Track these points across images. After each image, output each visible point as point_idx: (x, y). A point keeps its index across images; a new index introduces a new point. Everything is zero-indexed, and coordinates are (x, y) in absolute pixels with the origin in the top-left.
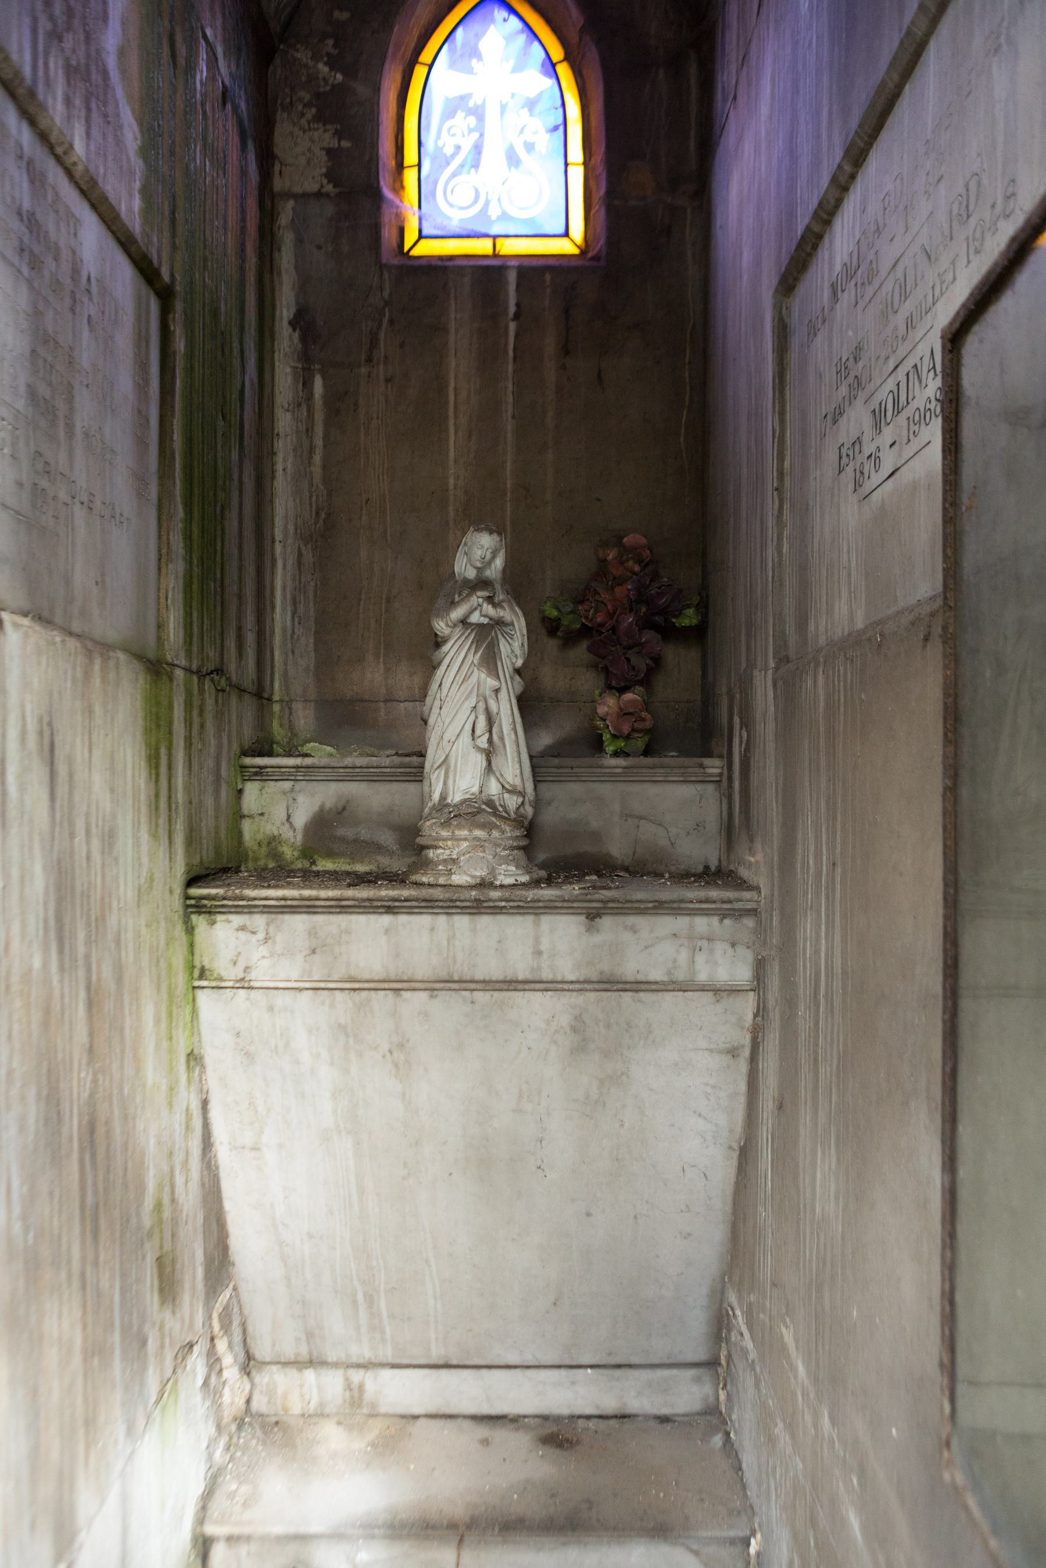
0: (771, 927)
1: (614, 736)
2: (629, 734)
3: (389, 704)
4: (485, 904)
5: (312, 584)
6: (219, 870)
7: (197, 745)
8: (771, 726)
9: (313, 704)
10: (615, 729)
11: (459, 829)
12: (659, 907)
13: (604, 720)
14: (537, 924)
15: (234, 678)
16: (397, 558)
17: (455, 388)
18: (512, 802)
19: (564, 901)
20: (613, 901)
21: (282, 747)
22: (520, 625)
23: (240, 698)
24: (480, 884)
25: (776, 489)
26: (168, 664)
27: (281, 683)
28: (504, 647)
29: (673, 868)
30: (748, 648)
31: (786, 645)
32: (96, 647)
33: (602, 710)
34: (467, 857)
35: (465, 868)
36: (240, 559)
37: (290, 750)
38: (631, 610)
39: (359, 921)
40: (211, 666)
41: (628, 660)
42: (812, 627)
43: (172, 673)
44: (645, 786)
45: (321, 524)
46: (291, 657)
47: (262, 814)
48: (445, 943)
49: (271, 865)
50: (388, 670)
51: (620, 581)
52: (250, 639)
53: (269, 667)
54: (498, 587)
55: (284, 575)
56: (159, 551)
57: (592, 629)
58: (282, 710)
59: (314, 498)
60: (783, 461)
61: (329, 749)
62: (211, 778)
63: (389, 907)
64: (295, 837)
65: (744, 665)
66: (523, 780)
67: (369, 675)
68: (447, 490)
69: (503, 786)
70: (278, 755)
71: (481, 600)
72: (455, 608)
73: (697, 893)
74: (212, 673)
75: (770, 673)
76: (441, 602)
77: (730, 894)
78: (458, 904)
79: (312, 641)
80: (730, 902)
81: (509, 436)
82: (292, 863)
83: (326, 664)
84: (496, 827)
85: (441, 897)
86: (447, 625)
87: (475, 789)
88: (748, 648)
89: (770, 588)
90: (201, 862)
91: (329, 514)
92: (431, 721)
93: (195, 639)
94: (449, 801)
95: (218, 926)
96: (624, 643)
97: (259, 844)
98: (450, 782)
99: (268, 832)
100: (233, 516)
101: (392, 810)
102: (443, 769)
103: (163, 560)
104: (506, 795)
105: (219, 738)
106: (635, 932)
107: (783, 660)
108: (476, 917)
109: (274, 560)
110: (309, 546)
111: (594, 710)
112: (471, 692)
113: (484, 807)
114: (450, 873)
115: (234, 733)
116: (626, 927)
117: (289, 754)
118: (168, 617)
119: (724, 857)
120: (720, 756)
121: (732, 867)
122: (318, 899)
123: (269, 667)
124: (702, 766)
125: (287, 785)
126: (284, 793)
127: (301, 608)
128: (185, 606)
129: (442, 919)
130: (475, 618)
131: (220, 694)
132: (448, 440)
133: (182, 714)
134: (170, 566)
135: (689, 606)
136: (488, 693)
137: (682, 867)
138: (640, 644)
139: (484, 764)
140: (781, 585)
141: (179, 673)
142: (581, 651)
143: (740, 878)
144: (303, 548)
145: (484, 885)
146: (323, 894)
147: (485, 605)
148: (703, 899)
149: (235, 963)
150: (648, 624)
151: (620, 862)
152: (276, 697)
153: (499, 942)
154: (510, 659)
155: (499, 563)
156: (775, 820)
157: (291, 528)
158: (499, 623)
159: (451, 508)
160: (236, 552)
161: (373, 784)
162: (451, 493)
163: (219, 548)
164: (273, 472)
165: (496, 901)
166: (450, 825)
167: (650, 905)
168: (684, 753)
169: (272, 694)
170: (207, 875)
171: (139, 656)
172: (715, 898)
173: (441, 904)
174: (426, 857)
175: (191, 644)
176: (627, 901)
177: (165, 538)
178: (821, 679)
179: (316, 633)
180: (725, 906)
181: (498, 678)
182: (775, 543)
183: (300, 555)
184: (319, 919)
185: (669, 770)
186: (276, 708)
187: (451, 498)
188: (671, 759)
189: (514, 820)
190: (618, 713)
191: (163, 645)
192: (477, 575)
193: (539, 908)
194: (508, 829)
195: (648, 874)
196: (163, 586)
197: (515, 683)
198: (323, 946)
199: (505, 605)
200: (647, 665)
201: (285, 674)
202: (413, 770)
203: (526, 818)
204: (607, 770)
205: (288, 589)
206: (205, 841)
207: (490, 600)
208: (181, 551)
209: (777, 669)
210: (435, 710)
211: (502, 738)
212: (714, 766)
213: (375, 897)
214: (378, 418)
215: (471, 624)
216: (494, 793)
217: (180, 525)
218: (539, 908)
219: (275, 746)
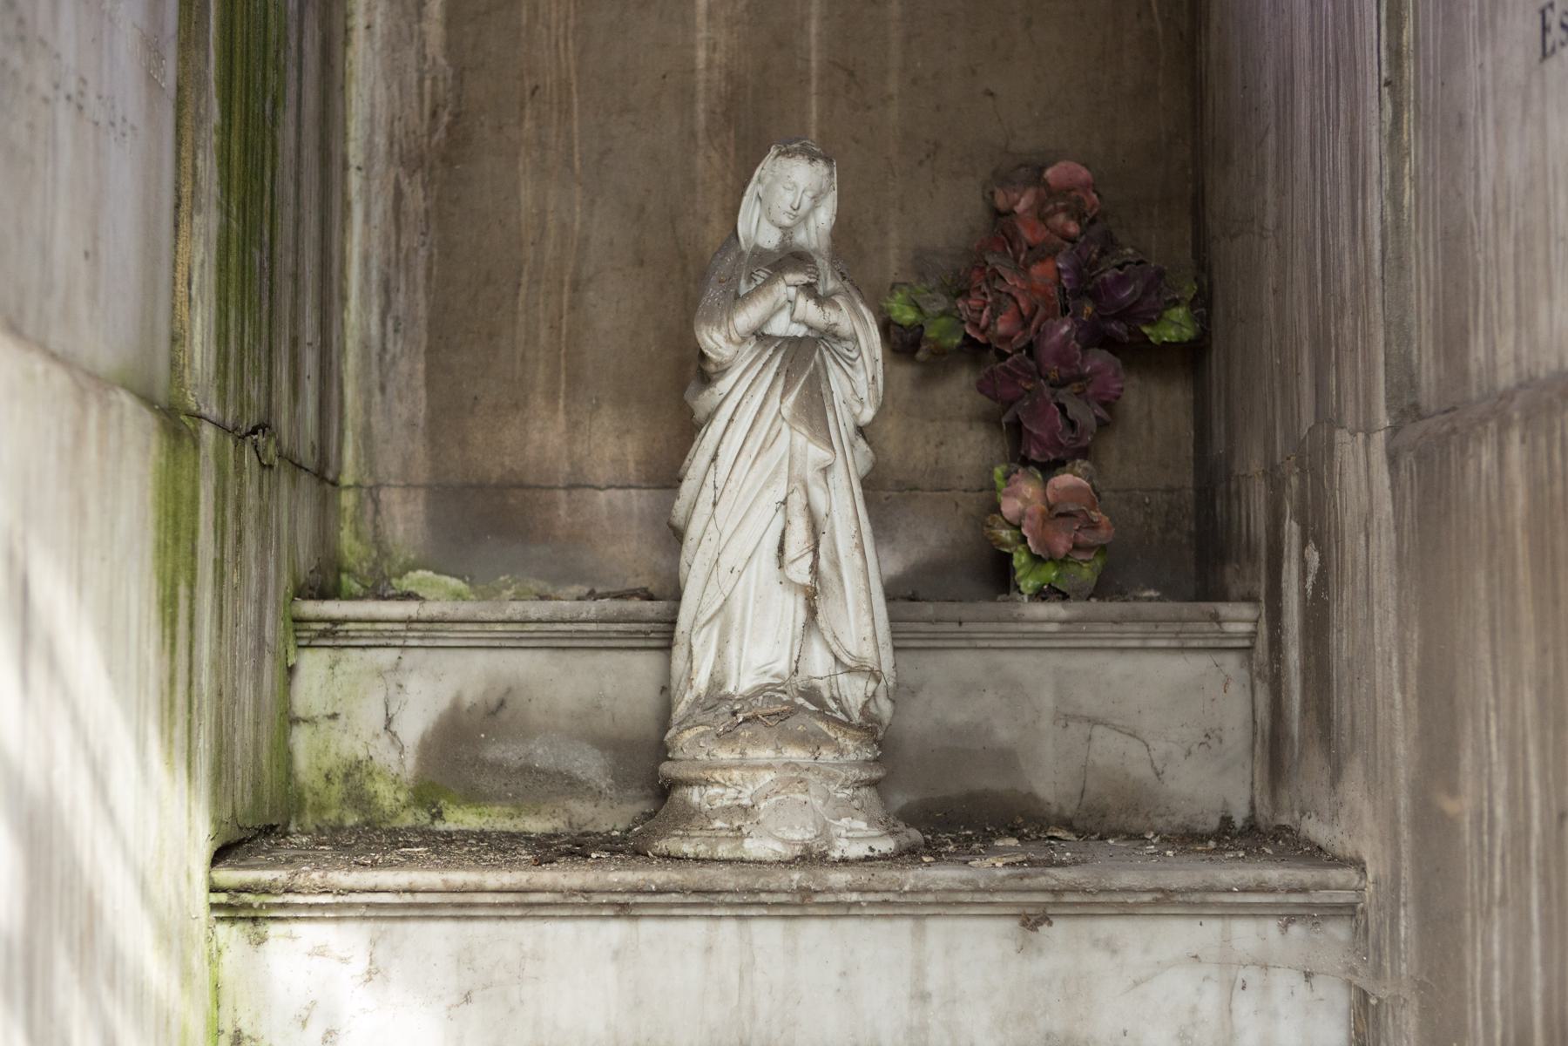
0: (1394, 942)
3: (576, 494)
4: (819, 898)
5: (422, 252)
6: (273, 828)
7: (233, 577)
8: (1384, 544)
9: (422, 493)
10: (1038, 545)
11: (756, 746)
12: (1165, 901)
13: (1019, 528)
14: (919, 937)
15: (285, 443)
16: (593, 202)
18: (855, 691)
19: (977, 890)
20: (1074, 890)
21: (360, 579)
22: (871, 339)
23: (294, 480)
24: (803, 858)
25: (1388, 84)
26: (190, 415)
27: (357, 449)
28: (837, 379)
29: (1160, 823)
30: (1319, 388)
31: (1414, 386)
32: (92, 382)
33: (1010, 507)
34: (775, 803)
35: (771, 826)
36: (298, 204)
37: (375, 587)
39: (561, 935)
40: (252, 419)
42: (1478, 351)
43: (197, 431)
44: (1101, 658)
45: (441, 134)
46: (377, 397)
47: (334, 716)
48: (735, 978)
49: (352, 819)
50: (573, 426)
51: (1040, 253)
52: (310, 360)
53: (335, 419)
54: (823, 264)
55: (367, 236)
56: (177, 190)
57: (988, 346)
58: (360, 504)
59: (428, 83)
60: (1400, 31)
61: (454, 583)
62: (251, 644)
63: (624, 906)
64: (401, 762)
65: (1308, 419)
66: (877, 648)
67: (535, 436)
68: (693, 71)
69: (836, 659)
70: (353, 597)
71: (792, 291)
73: (1239, 873)
74: (254, 431)
75: (1379, 438)
76: (713, 293)
77: (1306, 875)
78: (764, 897)
79: (421, 366)
80: (1303, 890)
82: (395, 815)
83: (447, 416)
84: (829, 741)
85: (731, 885)
86: (729, 339)
87: (783, 666)
88: (1319, 388)
89: (1378, 273)
90: (234, 815)
91: (456, 116)
92: (694, 531)
93: (232, 364)
94: (730, 689)
95: (271, 946)
96: (1053, 375)
97: (328, 778)
98: (732, 650)
99: (346, 751)
100: (288, 117)
101: (599, 707)
102: (717, 623)
103: (185, 207)
104: (843, 679)
105: (263, 564)
106: (1114, 952)
107: (1407, 412)
108: (798, 925)
109: (347, 206)
110: (418, 177)
111: (996, 509)
112: (776, 473)
113: (800, 701)
114: (738, 834)
115: (284, 551)
116: (1095, 943)
117: (377, 593)
118: (191, 320)
119: (1262, 802)
120: (1250, 598)
121: (1284, 820)
122: (480, 890)
123: (335, 419)
124: (1216, 618)
125: (386, 657)
126: (380, 674)
127: (400, 301)
128: (219, 299)
129: (728, 929)
130: (781, 326)
131: (266, 472)
133: (211, 515)
134: (197, 219)
136: (811, 474)
137: (1178, 820)
138: (1081, 377)
139: (802, 615)
140: (1401, 267)
141: (208, 433)
142: (960, 388)
143: (1309, 842)
144: (405, 183)
145: (810, 858)
146: (492, 879)
147: (801, 301)
148: (1253, 884)
149: (304, 1023)
150: (1096, 337)
151: (1054, 810)
152: (347, 478)
153: (844, 974)
154: (850, 409)
155: (825, 216)
156: (1400, 726)
157: (381, 140)
158: (828, 336)
160: (291, 190)
161: (560, 654)
162: (701, 76)
163: (267, 183)
164: (347, 31)
166: (735, 738)
167: (1147, 898)
168: (1170, 592)
169: (339, 473)
170: (240, 843)
171: (146, 399)
172: (1274, 883)
173: (729, 898)
174: (685, 802)
175: (225, 376)
176: (1102, 891)
177: (188, 163)
178: (1516, 452)
179: (429, 351)
180: (1295, 898)
181: (831, 445)
182: (1387, 185)
183: (399, 195)
184: (479, 931)
186: (348, 500)
187: (701, 87)
188: (1150, 605)
189: (860, 727)
190: (1043, 513)
191: (181, 376)
194: (850, 744)
195: (1114, 833)
196: (183, 259)
197: (857, 455)
198: (486, 987)
199: (838, 299)
200: (1097, 417)
201: (367, 434)
202: (643, 627)
203: (880, 723)
204: (1030, 627)
205: (374, 263)
206: (239, 772)
207: (809, 290)
208: (215, 190)
209: (1395, 430)
210: (704, 508)
211: (835, 564)
212: (1239, 619)
215: (772, 338)
217: (215, 138)
219: (344, 577)
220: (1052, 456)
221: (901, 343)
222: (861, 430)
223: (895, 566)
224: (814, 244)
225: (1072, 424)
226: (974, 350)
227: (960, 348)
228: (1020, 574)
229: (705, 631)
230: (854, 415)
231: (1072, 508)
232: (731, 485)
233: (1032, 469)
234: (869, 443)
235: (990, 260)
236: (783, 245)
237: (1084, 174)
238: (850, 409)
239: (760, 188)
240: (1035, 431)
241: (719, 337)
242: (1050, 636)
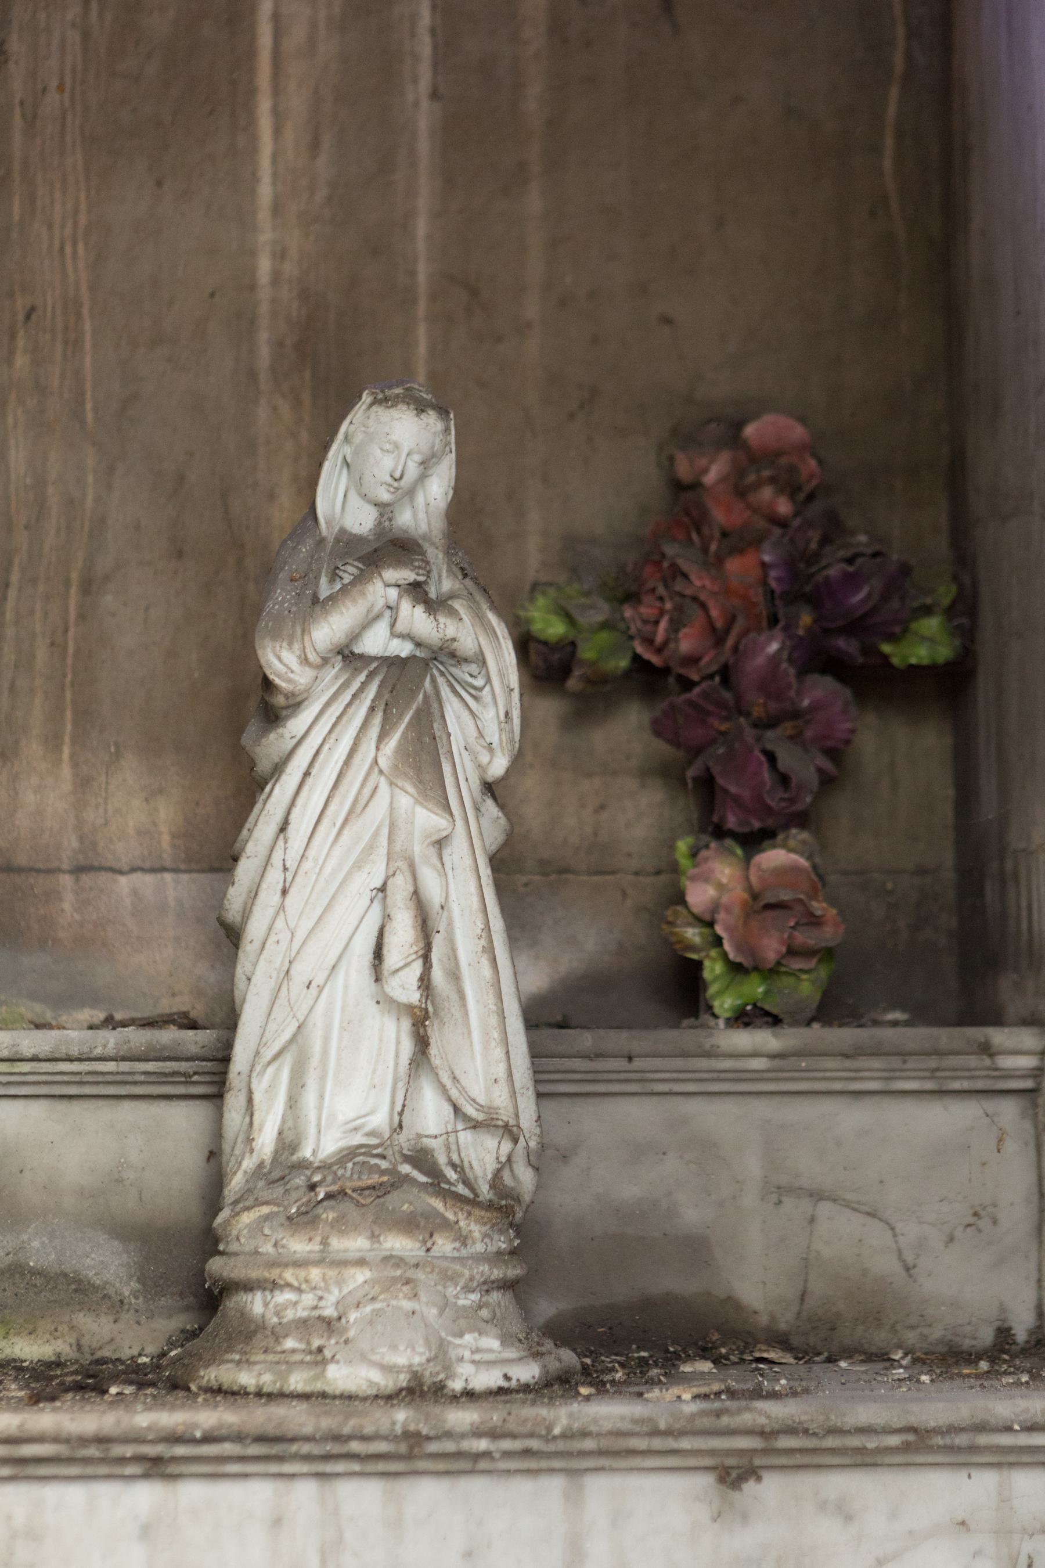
1: (736, 969)
2: (779, 963)
3: (86, 879)
4: (433, 1447)
10: (739, 948)
11: (342, 1233)
13: (711, 924)
14: (574, 1500)
16: (111, 470)
17: (276, 17)
18: (482, 1154)
19: (655, 1432)
20: (791, 1430)
22: (503, 661)
24: (410, 1391)
28: (455, 716)
29: (911, 1337)
34: (365, 1312)
38: (774, 621)
41: (771, 758)
50: (83, 783)
51: (737, 541)
54: (436, 555)
63: (157, 1461)
66: (513, 1094)
67: (30, 798)
71: (393, 593)
72: (326, 613)
76: (282, 597)
78: (355, 1446)
81: (424, 147)
84: (446, 1225)
85: (308, 1430)
86: (305, 661)
87: (380, 1120)
92: (255, 930)
94: (306, 1152)
96: (757, 712)
98: (309, 1098)
101: (120, 1181)
102: (288, 1060)
104: (466, 1137)
106: (849, 1518)
108: (404, 1486)
111: (680, 898)
112: (371, 847)
113: (406, 1169)
114: (319, 1358)
116: (822, 1506)
124: (986, 1049)
130: (377, 642)
132: (253, 149)
135: (927, 611)
136: (419, 849)
137: (937, 1333)
138: (796, 714)
139: (407, 1047)
142: (628, 731)
145: (420, 1391)
150: (817, 659)
151: (764, 1320)
154: (475, 757)
155: (438, 489)
158: (441, 656)
159: (263, 336)
161: (62, 1106)
162: (264, 294)
165: (463, 1436)
167: (894, 1440)
168: (923, 1014)
173: (305, 1448)
181: (447, 808)
185: (896, 1062)
187: (264, 308)
188: (895, 1031)
189: (490, 1206)
190: (744, 904)
192: (379, 524)
193: (583, 1454)
194: (476, 1230)
195: (848, 1353)
197: (485, 822)
199: (457, 605)
200: (820, 771)
202: (183, 1066)
207: (417, 591)
210: (268, 897)
211: (455, 976)
213: (116, 1432)
214: (61, 88)
216: (433, 1130)
218: (583, 1454)
220: (757, 825)
221: (546, 666)
222: (489, 788)
223: (538, 979)
224: (424, 528)
225: (784, 780)
226: (648, 678)
227: (627, 674)
228: (713, 989)
229: (270, 1070)
230: (480, 767)
231: (785, 896)
232: (307, 865)
233: (729, 842)
234: (502, 807)
235: (670, 550)
236: (380, 530)
237: (798, 432)
238: (475, 757)
239: (348, 450)
240: (733, 789)
241: (290, 657)
242: (757, 1076)
